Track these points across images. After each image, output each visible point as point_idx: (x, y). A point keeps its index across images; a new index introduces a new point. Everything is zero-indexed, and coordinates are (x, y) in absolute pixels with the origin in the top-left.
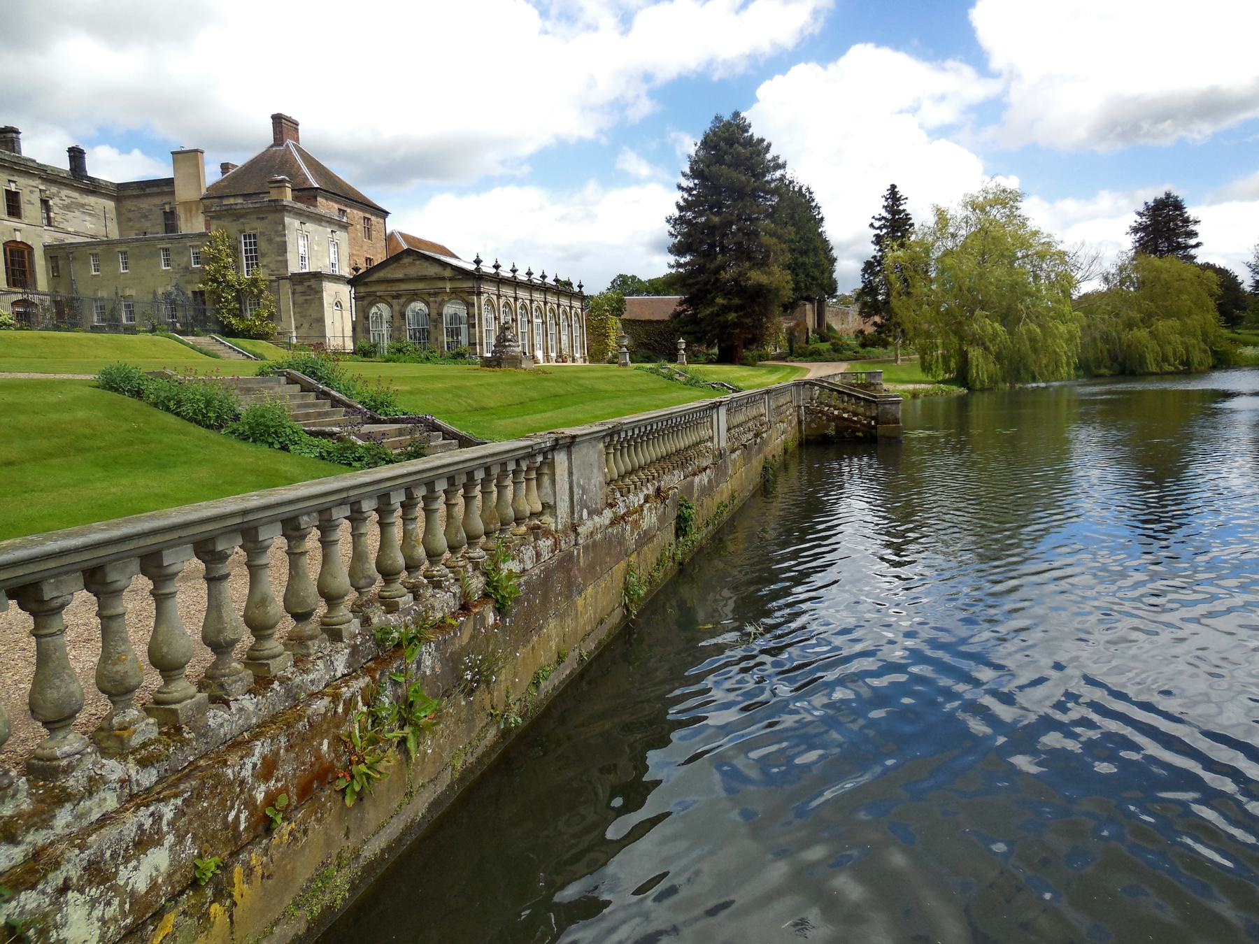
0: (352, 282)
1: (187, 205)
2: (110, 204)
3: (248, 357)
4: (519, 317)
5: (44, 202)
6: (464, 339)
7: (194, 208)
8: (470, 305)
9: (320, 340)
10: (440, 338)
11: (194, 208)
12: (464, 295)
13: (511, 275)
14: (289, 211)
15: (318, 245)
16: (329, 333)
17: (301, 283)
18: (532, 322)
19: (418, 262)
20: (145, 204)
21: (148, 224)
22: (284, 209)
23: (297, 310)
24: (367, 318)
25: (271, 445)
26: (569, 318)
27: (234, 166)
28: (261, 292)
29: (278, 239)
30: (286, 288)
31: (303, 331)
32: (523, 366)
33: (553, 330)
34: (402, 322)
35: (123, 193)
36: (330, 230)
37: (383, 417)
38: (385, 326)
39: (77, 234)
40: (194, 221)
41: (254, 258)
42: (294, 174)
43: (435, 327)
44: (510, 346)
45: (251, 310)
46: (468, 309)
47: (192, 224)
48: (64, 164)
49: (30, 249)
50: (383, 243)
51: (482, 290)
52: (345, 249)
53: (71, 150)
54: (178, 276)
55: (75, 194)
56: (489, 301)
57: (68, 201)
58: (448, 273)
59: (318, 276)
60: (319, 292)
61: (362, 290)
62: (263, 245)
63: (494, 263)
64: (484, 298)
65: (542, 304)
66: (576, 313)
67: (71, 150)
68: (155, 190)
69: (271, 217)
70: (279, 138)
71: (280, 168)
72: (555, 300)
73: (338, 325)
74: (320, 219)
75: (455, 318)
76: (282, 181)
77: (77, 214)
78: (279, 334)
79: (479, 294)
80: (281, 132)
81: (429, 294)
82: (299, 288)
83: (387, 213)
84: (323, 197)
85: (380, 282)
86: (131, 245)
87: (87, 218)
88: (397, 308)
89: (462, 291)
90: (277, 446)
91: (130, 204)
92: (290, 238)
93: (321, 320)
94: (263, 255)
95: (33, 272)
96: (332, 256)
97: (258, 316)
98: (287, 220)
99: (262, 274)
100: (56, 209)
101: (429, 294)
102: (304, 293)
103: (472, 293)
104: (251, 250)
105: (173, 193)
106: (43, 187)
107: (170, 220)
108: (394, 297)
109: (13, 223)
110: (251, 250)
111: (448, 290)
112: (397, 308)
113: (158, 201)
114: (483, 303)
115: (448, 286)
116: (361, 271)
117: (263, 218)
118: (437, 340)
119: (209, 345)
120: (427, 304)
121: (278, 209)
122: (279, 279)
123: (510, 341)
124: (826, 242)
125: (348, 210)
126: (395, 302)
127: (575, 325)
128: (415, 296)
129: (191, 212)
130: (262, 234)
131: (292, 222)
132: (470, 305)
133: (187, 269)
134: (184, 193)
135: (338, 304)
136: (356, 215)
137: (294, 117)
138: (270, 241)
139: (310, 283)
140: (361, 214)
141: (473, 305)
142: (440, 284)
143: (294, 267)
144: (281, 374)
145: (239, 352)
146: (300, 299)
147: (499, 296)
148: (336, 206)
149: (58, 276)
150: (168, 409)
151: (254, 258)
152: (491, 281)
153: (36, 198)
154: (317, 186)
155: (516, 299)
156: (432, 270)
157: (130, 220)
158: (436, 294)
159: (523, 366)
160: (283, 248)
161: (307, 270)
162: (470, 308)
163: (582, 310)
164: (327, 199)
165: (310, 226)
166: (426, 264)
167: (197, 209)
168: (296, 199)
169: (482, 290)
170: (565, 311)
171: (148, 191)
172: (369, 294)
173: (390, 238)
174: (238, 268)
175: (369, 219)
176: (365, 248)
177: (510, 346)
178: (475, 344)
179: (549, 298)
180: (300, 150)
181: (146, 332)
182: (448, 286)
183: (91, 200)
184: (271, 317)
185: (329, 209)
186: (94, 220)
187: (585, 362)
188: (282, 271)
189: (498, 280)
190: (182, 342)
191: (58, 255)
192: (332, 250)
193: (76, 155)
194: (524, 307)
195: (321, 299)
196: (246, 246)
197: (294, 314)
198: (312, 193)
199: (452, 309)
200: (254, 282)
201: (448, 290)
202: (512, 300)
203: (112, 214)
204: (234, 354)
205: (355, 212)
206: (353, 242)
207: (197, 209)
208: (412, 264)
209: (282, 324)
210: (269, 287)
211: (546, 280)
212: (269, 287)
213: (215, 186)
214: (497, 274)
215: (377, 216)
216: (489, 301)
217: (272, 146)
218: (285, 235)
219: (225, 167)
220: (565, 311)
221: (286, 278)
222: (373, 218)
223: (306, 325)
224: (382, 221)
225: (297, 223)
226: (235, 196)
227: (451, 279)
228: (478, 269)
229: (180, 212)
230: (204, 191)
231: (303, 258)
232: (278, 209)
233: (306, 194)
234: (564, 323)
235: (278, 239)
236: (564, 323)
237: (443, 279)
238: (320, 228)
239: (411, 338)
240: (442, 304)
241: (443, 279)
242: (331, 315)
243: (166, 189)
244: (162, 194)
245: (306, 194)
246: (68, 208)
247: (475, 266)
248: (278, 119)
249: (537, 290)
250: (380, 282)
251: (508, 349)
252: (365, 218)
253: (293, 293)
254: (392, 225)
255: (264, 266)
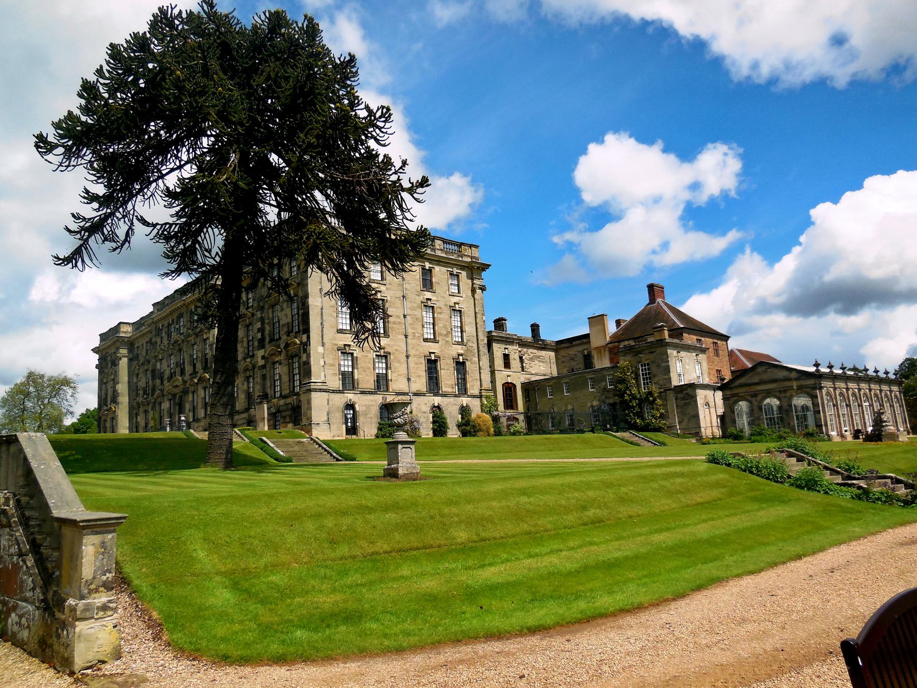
0: (722, 388)
1: (598, 349)
2: (552, 354)
3: (655, 444)
4: (839, 402)
5: (521, 358)
6: (811, 421)
7: (602, 351)
8: (814, 397)
9: (697, 430)
10: (792, 423)
11: (602, 351)
12: (808, 390)
13: (885, 376)
14: (669, 346)
15: (688, 365)
16: (702, 424)
17: (681, 392)
18: (862, 406)
19: (769, 370)
20: (572, 351)
21: (574, 364)
22: (668, 344)
23: (679, 410)
24: (733, 412)
25: (819, 491)
26: (890, 400)
27: (625, 321)
28: (655, 400)
29: (663, 364)
30: (671, 396)
31: (684, 424)
32: (900, 439)
33: (844, 410)
34: (760, 413)
35: (560, 346)
36: (695, 354)
37: (857, 476)
38: (745, 417)
39: (536, 374)
40: (603, 358)
41: (649, 378)
42: (667, 320)
43: (787, 415)
44: (887, 426)
45: (648, 413)
46: (813, 401)
47: (602, 362)
48: (527, 334)
49: (515, 386)
50: (727, 358)
51: (823, 385)
52: (705, 365)
53: (532, 326)
54: (599, 395)
55: (535, 351)
56: (828, 394)
57: (532, 355)
58: (794, 375)
59: (692, 386)
60: (694, 397)
61: (728, 392)
62: (654, 370)
63: (828, 364)
64: (824, 391)
65: (867, 391)
66: (896, 396)
67: (532, 326)
68: (578, 342)
69: (659, 350)
70: (652, 300)
71: (655, 318)
72: (843, 385)
73: (708, 418)
74: (688, 348)
75: (805, 408)
76: (662, 326)
77: (536, 362)
78: (668, 427)
79: (821, 388)
80: (654, 295)
81: (780, 392)
82: (680, 395)
83: (728, 337)
84: (686, 333)
85: (741, 386)
86: (571, 378)
87: (541, 364)
88: (755, 404)
89: (807, 387)
90: (822, 492)
91: (563, 353)
92: (672, 362)
93: (697, 416)
94: (655, 376)
95: (516, 399)
96: (697, 371)
97: (653, 416)
98: (669, 351)
99: (655, 389)
100: (526, 361)
101: (780, 392)
102: (683, 399)
103: (815, 388)
104: (646, 374)
105: (589, 342)
106: (520, 349)
107: (588, 360)
108: (752, 396)
109: (507, 372)
110: (646, 374)
111: (795, 388)
112: (755, 404)
113: (580, 348)
114: (824, 394)
115: (795, 384)
116: (725, 381)
117: (653, 352)
118: (789, 424)
119: (630, 437)
120: (779, 399)
121: (662, 343)
122: (666, 391)
123: (886, 422)
124: (675, 30)
125: (703, 339)
126: (754, 399)
127: (896, 405)
128: (769, 394)
129: (601, 353)
130: (653, 362)
131: (672, 352)
132: (814, 397)
133: (605, 389)
134: (596, 342)
135: (707, 404)
136: (707, 342)
137: (661, 284)
138: (658, 366)
139: (687, 392)
140: (711, 340)
141: (817, 397)
142: (788, 384)
143: (675, 382)
144: (782, 452)
145: (649, 441)
146: (681, 403)
147: (835, 389)
148: (695, 337)
149: (529, 401)
150: (752, 473)
151: (649, 378)
152: (829, 378)
153: (517, 356)
154: (682, 326)
155: (847, 389)
156: (785, 373)
157: (563, 362)
158: (785, 391)
159: (900, 439)
160: (667, 370)
161: (683, 383)
162: (815, 399)
163: (900, 392)
164: (689, 334)
165: (683, 354)
166: (776, 371)
167: (605, 351)
168: (670, 336)
169: (823, 385)
170: (886, 395)
171: (574, 343)
172: (733, 396)
173: (731, 354)
174: (638, 386)
175: (716, 343)
176: (716, 363)
177: (887, 426)
178: (821, 426)
179: (873, 386)
180: (666, 304)
181: (588, 431)
182: (795, 384)
183: (543, 353)
184: (662, 416)
185: (691, 340)
186: (545, 365)
187: (909, 434)
188: (668, 385)
189: (833, 377)
190: (615, 436)
191: (529, 388)
192: (697, 367)
193: (535, 328)
194: (854, 394)
195: (696, 401)
196: (642, 371)
197: (678, 413)
198: (680, 331)
199: (801, 401)
200: (650, 393)
201: (795, 388)
202: (844, 390)
203: (554, 360)
204: (646, 443)
205: (707, 339)
206: (709, 361)
207: (605, 351)
208: (765, 371)
209: (669, 420)
210: (660, 397)
211: (879, 374)
212: (660, 397)
213: (614, 336)
214: (832, 372)
215: (722, 340)
216: (828, 394)
217: (648, 305)
218: (668, 361)
219: (618, 323)
220: (886, 395)
221: (671, 389)
222: (719, 342)
223: (686, 420)
224: (725, 343)
225: (675, 352)
226: (628, 340)
227: (796, 379)
228: (818, 371)
229: (595, 354)
230: (608, 339)
231: (680, 375)
232: (662, 343)
233: (677, 333)
234: (854, 405)
235: (663, 364)
236: (854, 405)
237: (790, 380)
238: (689, 354)
239: (768, 425)
240: (791, 398)
241: (790, 380)
242: (703, 412)
243: (584, 340)
244: (582, 344)
245: (677, 333)
246: (531, 359)
247: (815, 368)
248: (651, 287)
249: (863, 380)
250: (741, 386)
251: (886, 428)
252: (697, 340)
253: (676, 399)
254: (732, 344)
255: (655, 383)
